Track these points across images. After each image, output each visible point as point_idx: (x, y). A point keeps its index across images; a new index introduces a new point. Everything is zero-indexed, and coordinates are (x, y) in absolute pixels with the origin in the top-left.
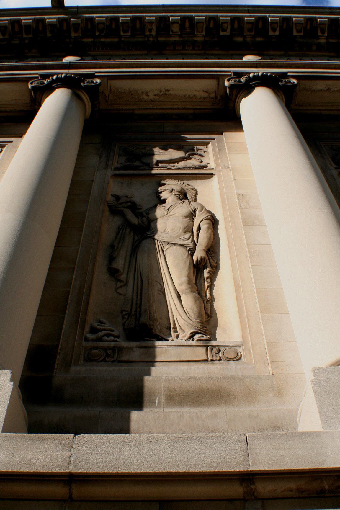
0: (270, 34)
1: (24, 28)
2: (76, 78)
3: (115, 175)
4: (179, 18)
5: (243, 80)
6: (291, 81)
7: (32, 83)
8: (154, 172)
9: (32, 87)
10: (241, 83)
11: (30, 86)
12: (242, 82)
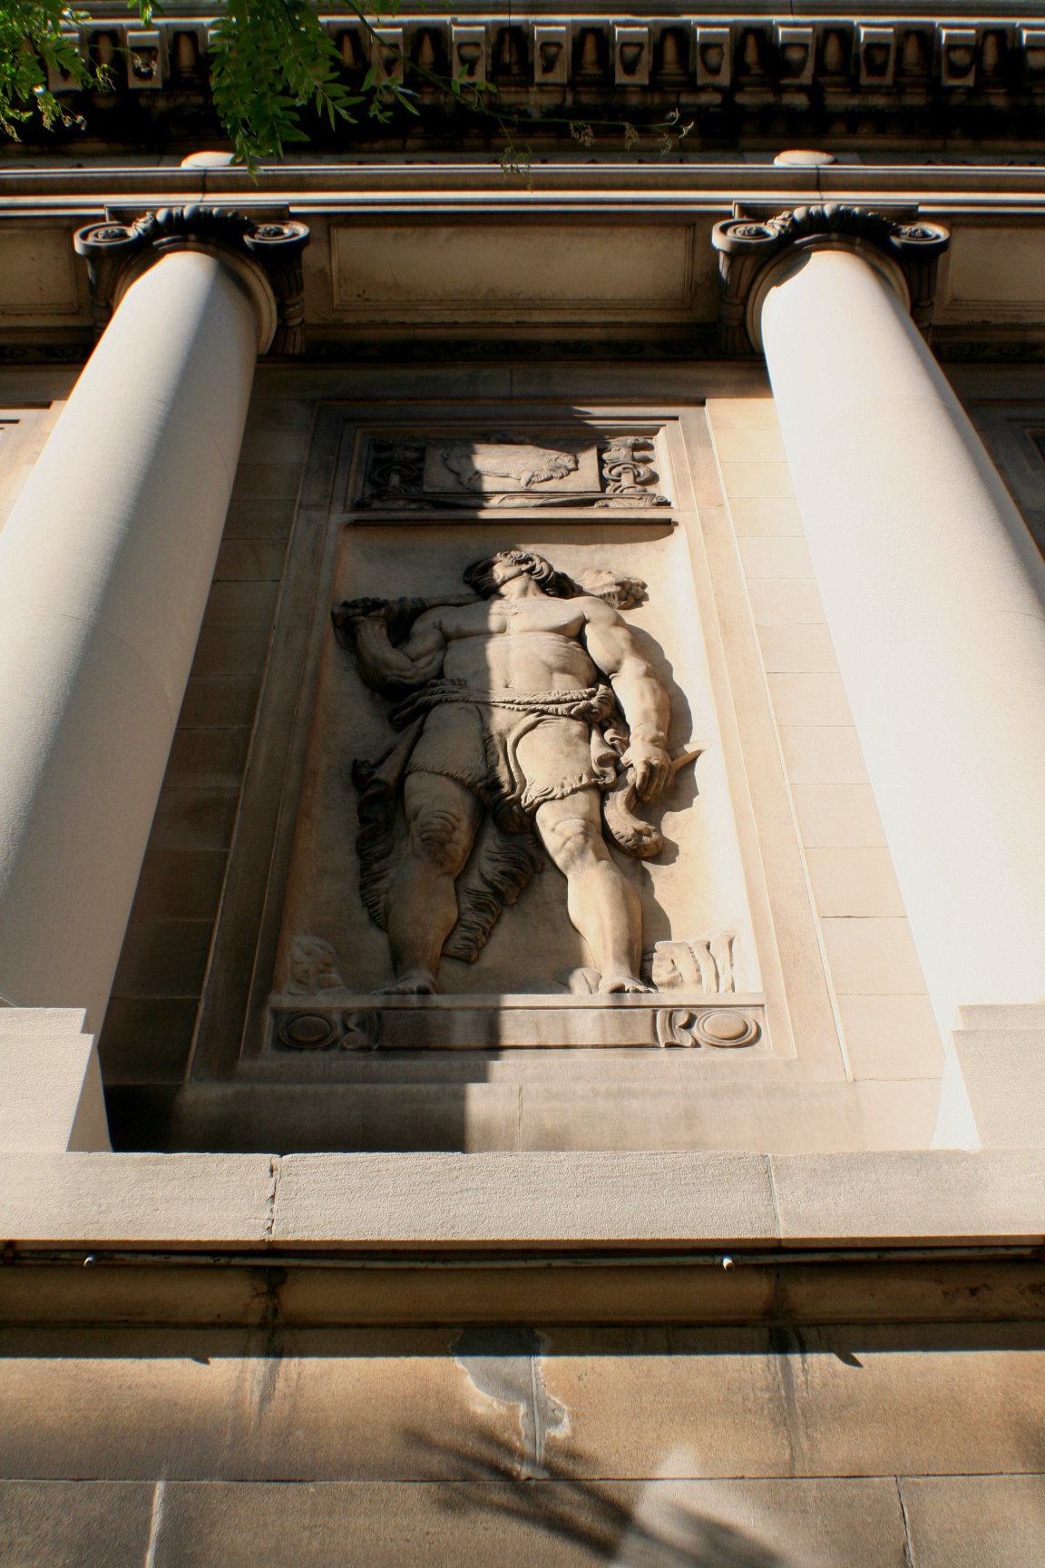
0: (618, 81)
1: (698, 46)
2: (794, 221)
3: (355, 524)
4: (76, 35)
5: (773, 228)
6: (930, 233)
7: (84, 236)
8: (484, 515)
9: (87, 247)
10: (126, 241)
11: (79, 246)
12: (768, 236)
